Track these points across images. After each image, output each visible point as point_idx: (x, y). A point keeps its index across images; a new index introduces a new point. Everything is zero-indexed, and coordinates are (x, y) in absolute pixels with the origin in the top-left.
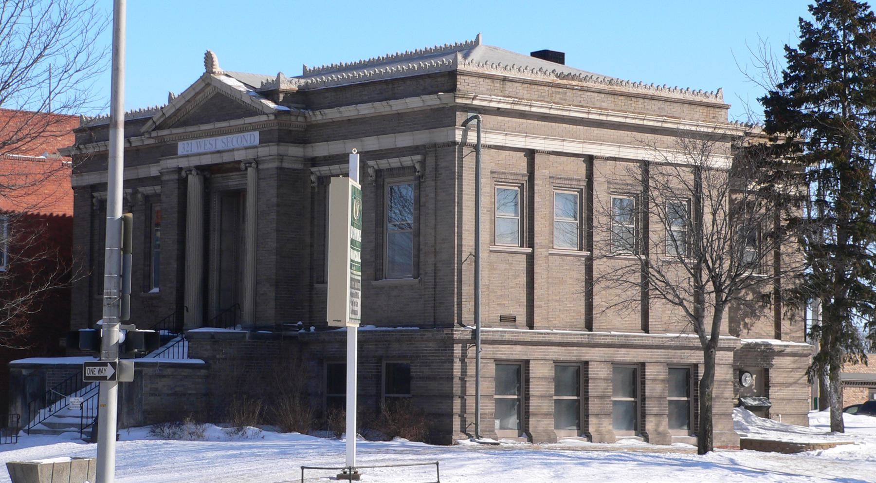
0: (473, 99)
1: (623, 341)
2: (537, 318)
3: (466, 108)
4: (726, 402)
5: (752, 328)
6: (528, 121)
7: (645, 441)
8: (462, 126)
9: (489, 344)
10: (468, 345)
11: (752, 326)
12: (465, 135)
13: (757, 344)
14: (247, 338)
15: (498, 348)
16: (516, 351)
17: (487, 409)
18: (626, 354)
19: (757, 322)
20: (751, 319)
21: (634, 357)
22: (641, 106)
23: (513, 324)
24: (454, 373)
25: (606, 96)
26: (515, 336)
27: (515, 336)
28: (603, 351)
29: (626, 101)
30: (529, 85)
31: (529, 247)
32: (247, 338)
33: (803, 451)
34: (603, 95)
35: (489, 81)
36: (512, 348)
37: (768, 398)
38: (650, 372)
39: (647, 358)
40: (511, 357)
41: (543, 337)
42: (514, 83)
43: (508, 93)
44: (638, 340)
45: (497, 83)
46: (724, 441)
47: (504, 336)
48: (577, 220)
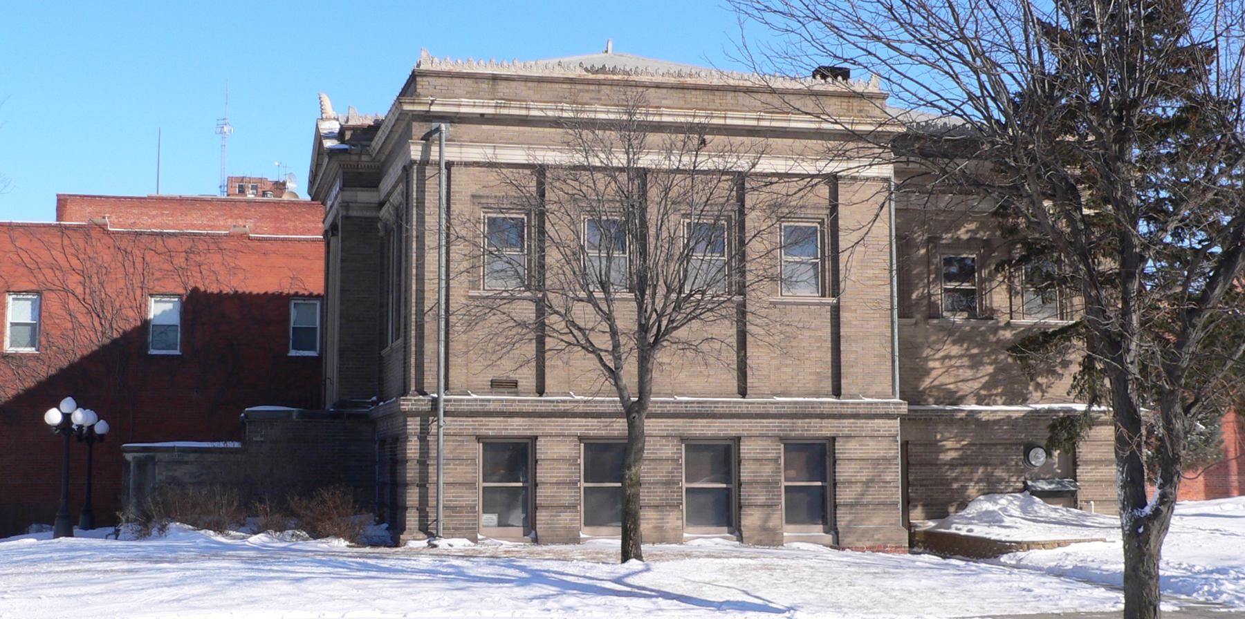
0: (431, 105)
1: (696, 409)
2: (549, 382)
3: (428, 117)
4: (886, 487)
5: (1049, 389)
6: (533, 129)
7: (738, 540)
8: (422, 139)
9: (467, 417)
10: (431, 418)
11: (1049, 387)
12: (426, 151)
13: (1050, 411)
14: (294, 417)
15: (482, 421)
16: (513, 425)
17: (464, 501)
18: (706, 426)
19: (1058, 381)
20: (1046, 378)
21: (719, 430)
22: (732, 102)
23: (513, 390)
24: (408, 455)
25: (670, 91)
26: (505, 406)
27: (505, 406)
28: (663, 422)
29: (706, 97)
30: (536, 84)
31: (833, 296)
32: (294, 417)
33: (1012, 552)
34: (665, 91)
35: (469, 82)
36: (507, 422)
37: (1076, 480)
38: (747, 449)
39: (743, 430)
40: (504, 433)
41: (554, 406)
42: (512, 83)
43: (501, 94)
44: (722, 407)
45: (484, 82)
46: (879, 540)
47: (486, 405)
48: (724, 256)
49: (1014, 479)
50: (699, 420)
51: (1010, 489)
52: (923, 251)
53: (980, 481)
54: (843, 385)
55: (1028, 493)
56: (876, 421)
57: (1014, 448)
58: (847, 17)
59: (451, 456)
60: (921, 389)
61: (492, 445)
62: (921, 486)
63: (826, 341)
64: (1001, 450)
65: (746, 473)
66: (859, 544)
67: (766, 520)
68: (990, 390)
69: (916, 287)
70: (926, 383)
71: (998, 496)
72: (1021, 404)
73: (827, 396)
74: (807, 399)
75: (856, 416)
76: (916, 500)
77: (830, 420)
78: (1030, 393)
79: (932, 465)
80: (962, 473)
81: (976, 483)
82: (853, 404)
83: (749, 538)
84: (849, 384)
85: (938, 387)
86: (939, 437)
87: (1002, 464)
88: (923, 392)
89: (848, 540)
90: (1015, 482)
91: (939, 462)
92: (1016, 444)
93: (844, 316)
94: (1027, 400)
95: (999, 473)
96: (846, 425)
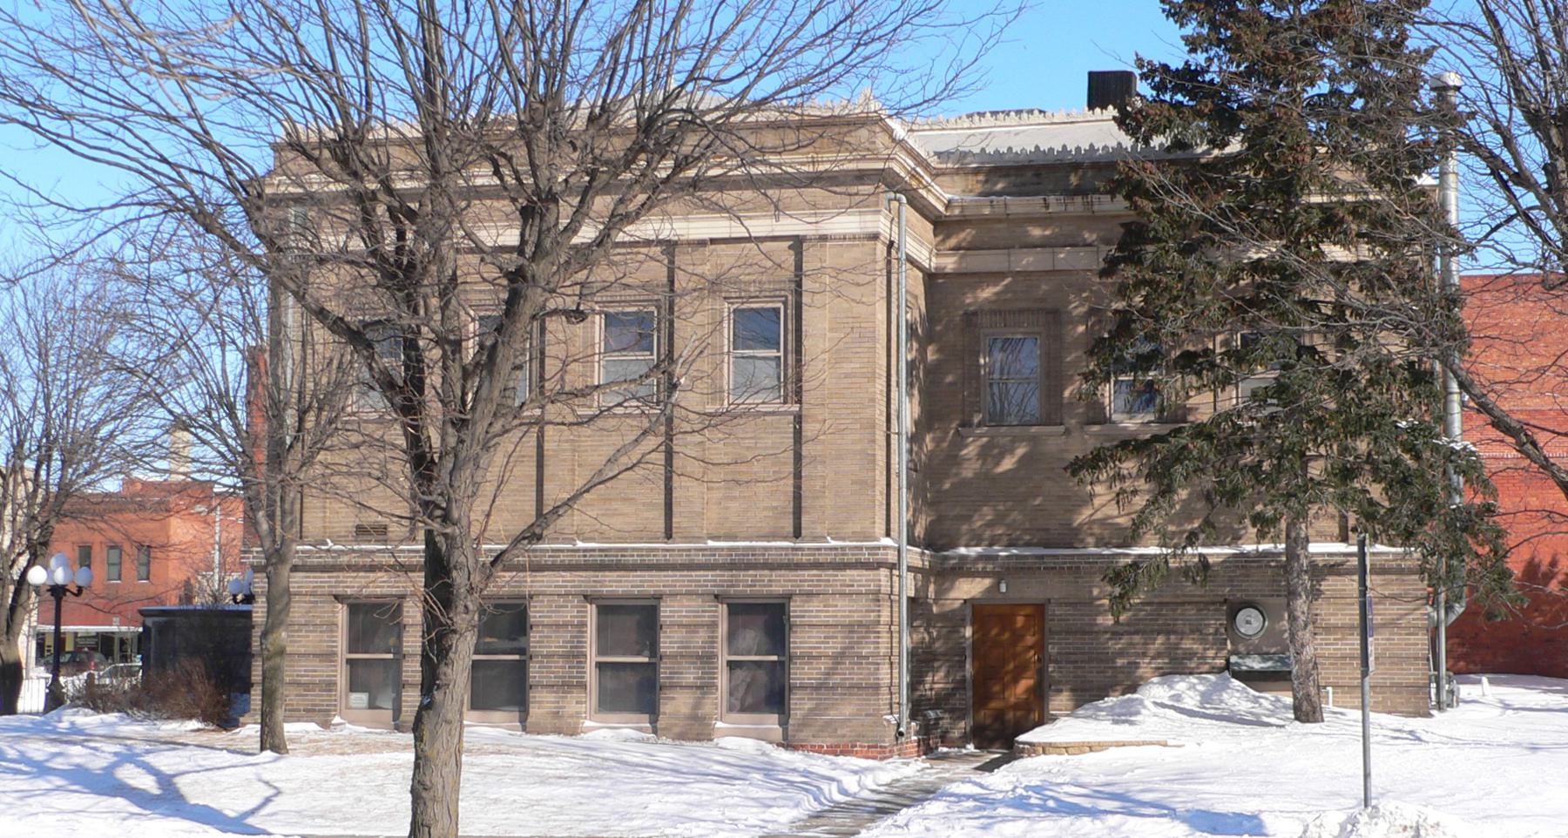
23: (381, 537)
38: (667, 612)
46: (844, 736)
49: (1211, 653)
50: (607, 573)
51: (1206, 668)
52: (1081, 329)
53: (1158, 655)
54: (803, 525)
55: (1226, 673)
56: (848, 572)
57: (1212, 608)
58: (86, 84)
59: (303, 621)
60: (1075, 524)
61: (610, 609)
62: (1067, 662)
63: (785, 463)
64: (1191, 611)
65: (669, 642)
66: (817, 742)
67: (697, 705)
68: (1182, 525)
69: (1070, 380)
70: (1084, 515)
71: (1177, 678)
72: (1229, 545)
73: (785, 538)
74: (754, 544)
75: (817, 566)
76: (1059, 682)
77: (783, 572)
78: (1245, 528)
79: (1084, 633)
80: (1131, 644)
81: (1153, 658)
82: (809, 549)
83: (664, 729)
84: (813, 522)
85: (1103, 522)
86: (1096, 592)
87: (1192, 632)
88: (1078, 529)
89: (804, 735)
90: (1214, 658)
91: (1096, 629)
92: (1213, 603)
93: (809, 429)
94: (1240, 538)
95: (1187, 644)
96: (807, 579)
